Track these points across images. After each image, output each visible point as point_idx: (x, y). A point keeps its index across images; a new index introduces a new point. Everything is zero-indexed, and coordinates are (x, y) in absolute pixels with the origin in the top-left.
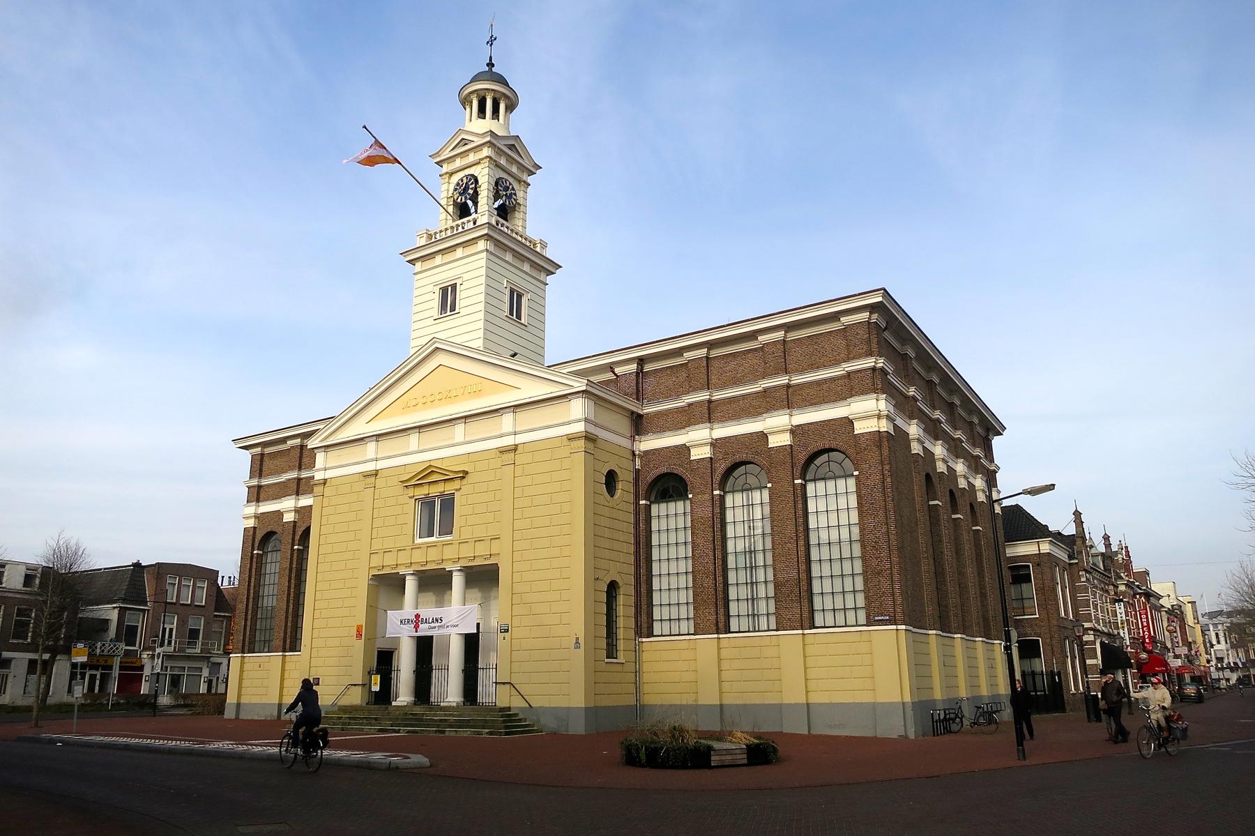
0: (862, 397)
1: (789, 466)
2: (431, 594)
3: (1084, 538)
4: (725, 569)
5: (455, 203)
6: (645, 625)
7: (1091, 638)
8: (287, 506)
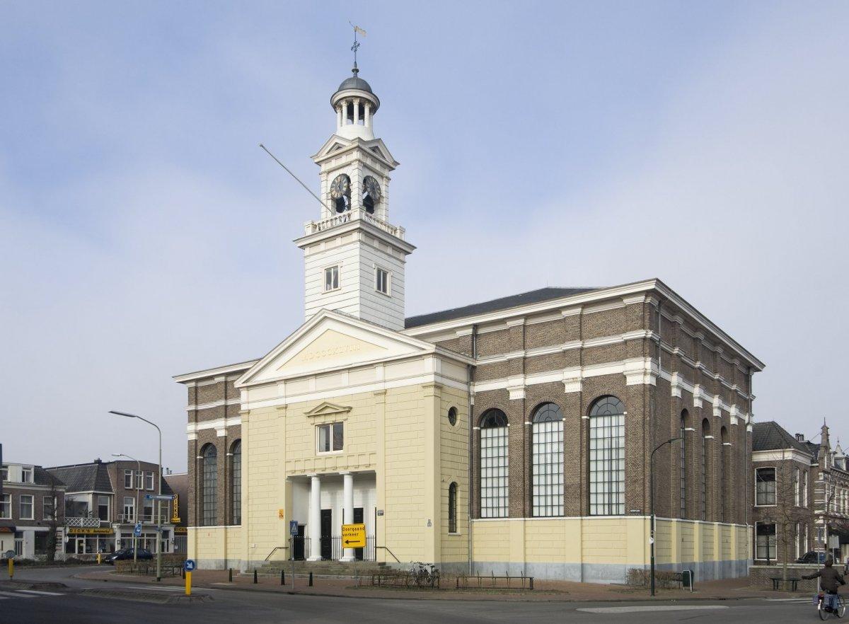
0: (635, 359)
1: (578, 406)
2: (327, 492)
3: (827, 448)
4: (531, 475)
5: (333, 199)
6: (475, 511)
7: (821, 521)
8: (220, 426)
